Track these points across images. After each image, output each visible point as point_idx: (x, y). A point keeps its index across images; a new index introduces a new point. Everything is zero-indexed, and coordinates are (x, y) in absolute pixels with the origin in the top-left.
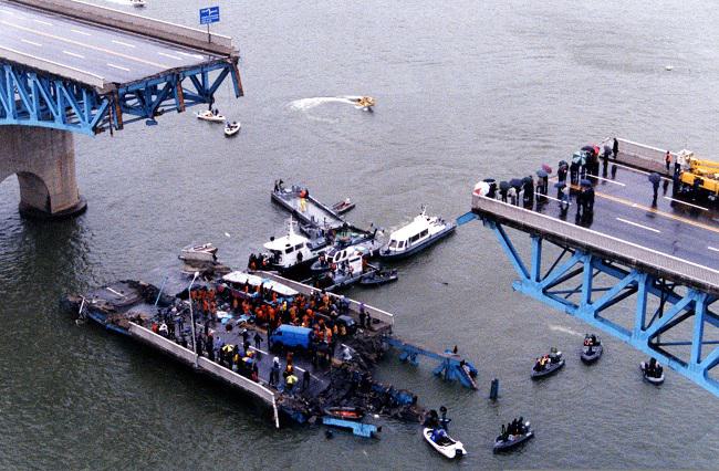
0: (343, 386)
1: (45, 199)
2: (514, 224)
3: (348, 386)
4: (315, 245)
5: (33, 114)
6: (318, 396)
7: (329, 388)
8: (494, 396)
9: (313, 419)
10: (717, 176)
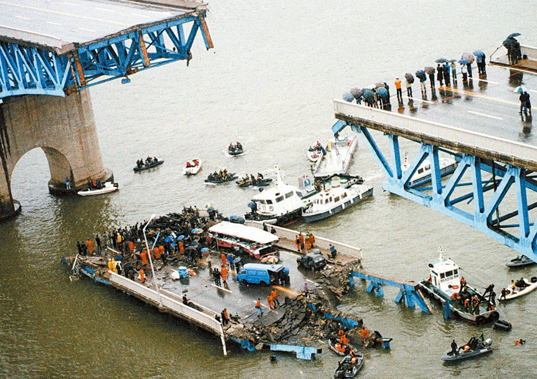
0: (296, 316)
1: (69, 171)
2: (376, 126)
3: (302, 316)
4: (305, 194)
5: (38, 83)
6: (270, 326)
7: (283, 318)
8: (222, 225)
9: (259, 346)
10: (2, 29)
